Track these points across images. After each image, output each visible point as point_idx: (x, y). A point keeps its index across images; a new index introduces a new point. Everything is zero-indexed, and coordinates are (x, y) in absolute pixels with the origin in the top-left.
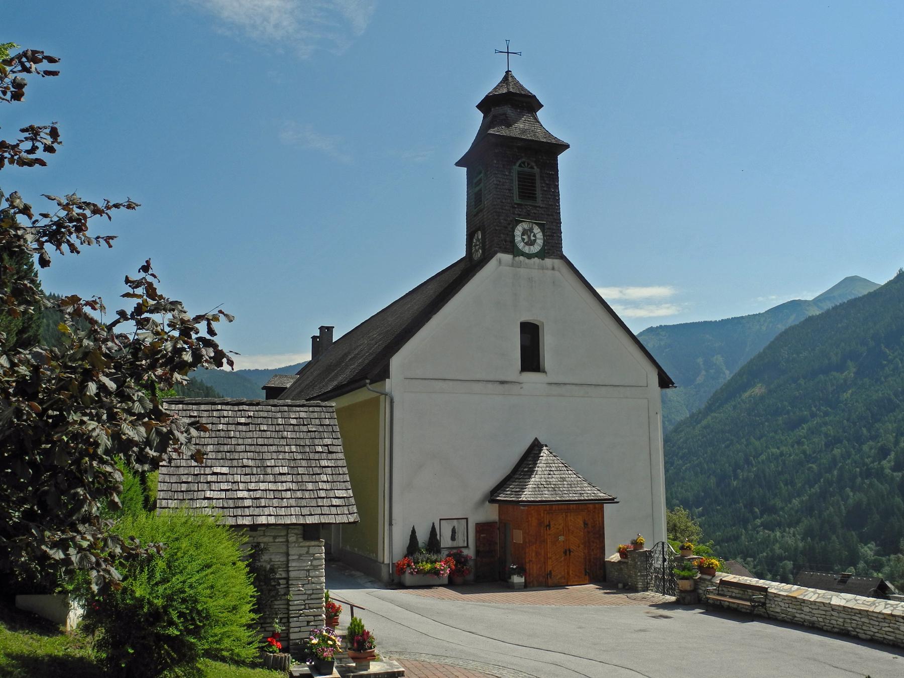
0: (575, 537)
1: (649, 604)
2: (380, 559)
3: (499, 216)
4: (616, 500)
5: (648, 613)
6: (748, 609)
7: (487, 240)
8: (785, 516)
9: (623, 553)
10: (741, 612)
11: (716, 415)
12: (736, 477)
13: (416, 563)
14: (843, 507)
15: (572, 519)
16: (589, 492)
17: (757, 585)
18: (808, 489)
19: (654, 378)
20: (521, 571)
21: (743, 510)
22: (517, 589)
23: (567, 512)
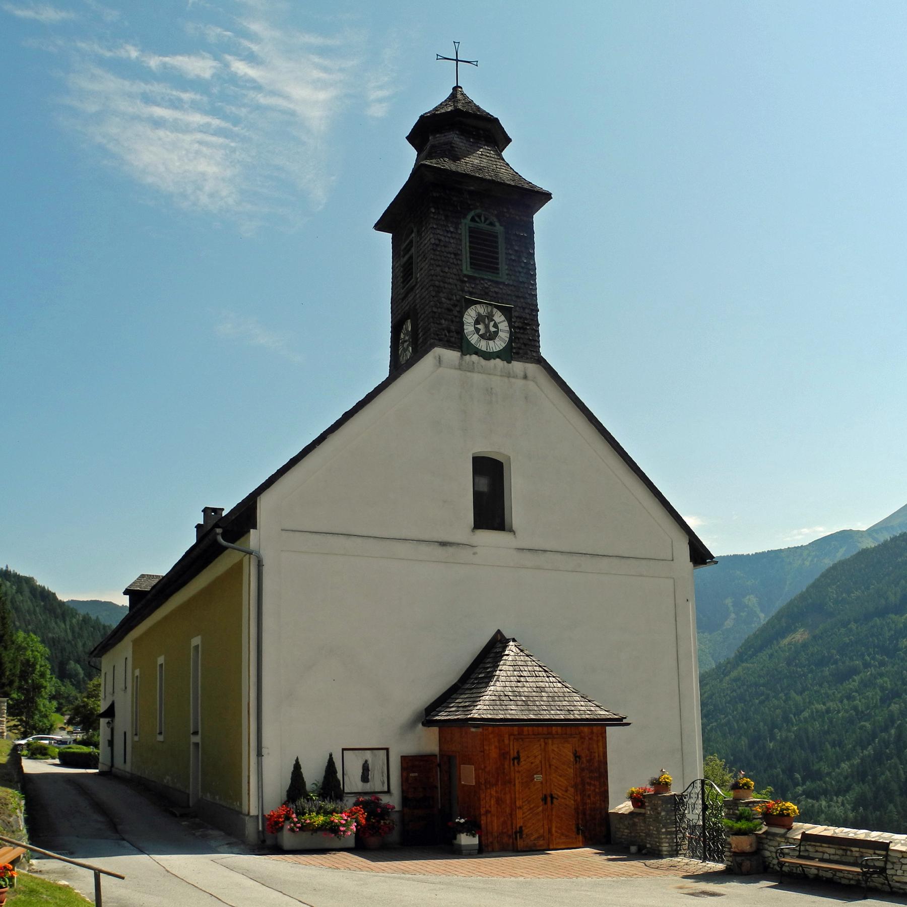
0: (560, 776)
1: (681, 876)
2: (245, 810)
3: (439, 292)
4: (625, 721)
5: (681, 888)
6: (852, 879)
7: (420, 330)
8: (831, 783)
9: (637, 799)
10: (840, 883)
11: (748, 665)
12: (773, 738)
13: (301, 813)
14: (902, 772)
15: (555, 749)
16: (583, 708)
17: (869, 839)
18: (861, 751)
19: (683, 550)
20: (472, 827)
21: (781, 776)
22: (465, 855)
23: (548, 738)
